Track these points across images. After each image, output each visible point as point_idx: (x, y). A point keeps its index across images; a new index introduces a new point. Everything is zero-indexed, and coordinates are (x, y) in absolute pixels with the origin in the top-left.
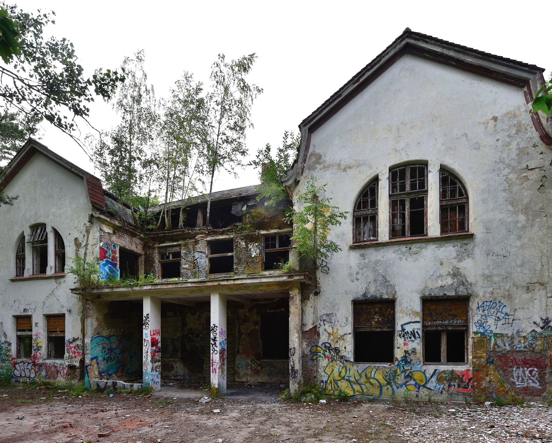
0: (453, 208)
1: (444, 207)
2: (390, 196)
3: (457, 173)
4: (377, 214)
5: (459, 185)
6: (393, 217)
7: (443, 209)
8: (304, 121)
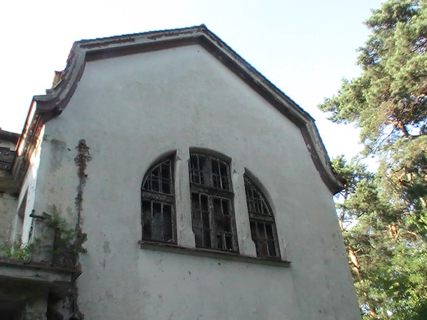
8: (83, 41)
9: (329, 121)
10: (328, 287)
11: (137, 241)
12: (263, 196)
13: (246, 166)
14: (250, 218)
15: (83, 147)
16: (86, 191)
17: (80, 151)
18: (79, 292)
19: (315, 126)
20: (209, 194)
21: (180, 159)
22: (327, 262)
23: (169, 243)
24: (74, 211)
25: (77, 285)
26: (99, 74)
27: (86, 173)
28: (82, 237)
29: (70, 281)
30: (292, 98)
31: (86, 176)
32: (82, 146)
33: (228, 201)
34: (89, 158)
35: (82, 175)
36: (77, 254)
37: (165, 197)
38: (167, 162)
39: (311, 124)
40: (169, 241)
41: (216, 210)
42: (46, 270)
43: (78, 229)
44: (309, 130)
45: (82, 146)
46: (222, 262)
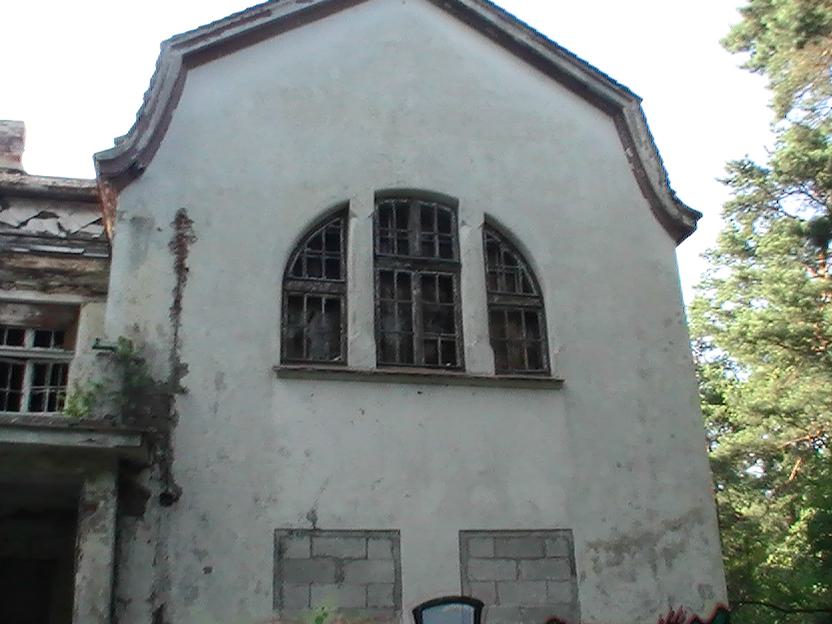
0: (515, 316)
1: (496, 308)
2: (376, 257)
3: (518, 241)
4: (344, 293)
5: (521, 266)
6: (382, 312)
7: (496, 316)
8: (175, 38)
9: (743, 70)
10: (642, 420)
11: (272, 365)
12: (525, 261)
13: (486, 211)
14: (490, 306)
15: (183, 220)
16: (186, 293)
17: (178, 228)
18: (176, 454)
19: (640, 110)
20: (414, 270)
21: (355, 216)
22: (644, 374)
23: (336, 363)
24: (168, 329)
25: (173, 444)
26: (208, 87)
27: (187, 266)
28: (179, 370)
29: (139, 444)
30: (591, 63)
31: (187, 269)
32: (181, 220)
33: (451, 277)
34: (192, 239)
35: (181, 269)
36: (172, 397)
37: (329, 284)
38: (334, 224)
39: (633, 108)
40: (336, 359)
41: (427, 294)
42: (104, 431)
43: (174, 358)
44: (628, 121)
45: (181, 220)
46: (424, 389)
